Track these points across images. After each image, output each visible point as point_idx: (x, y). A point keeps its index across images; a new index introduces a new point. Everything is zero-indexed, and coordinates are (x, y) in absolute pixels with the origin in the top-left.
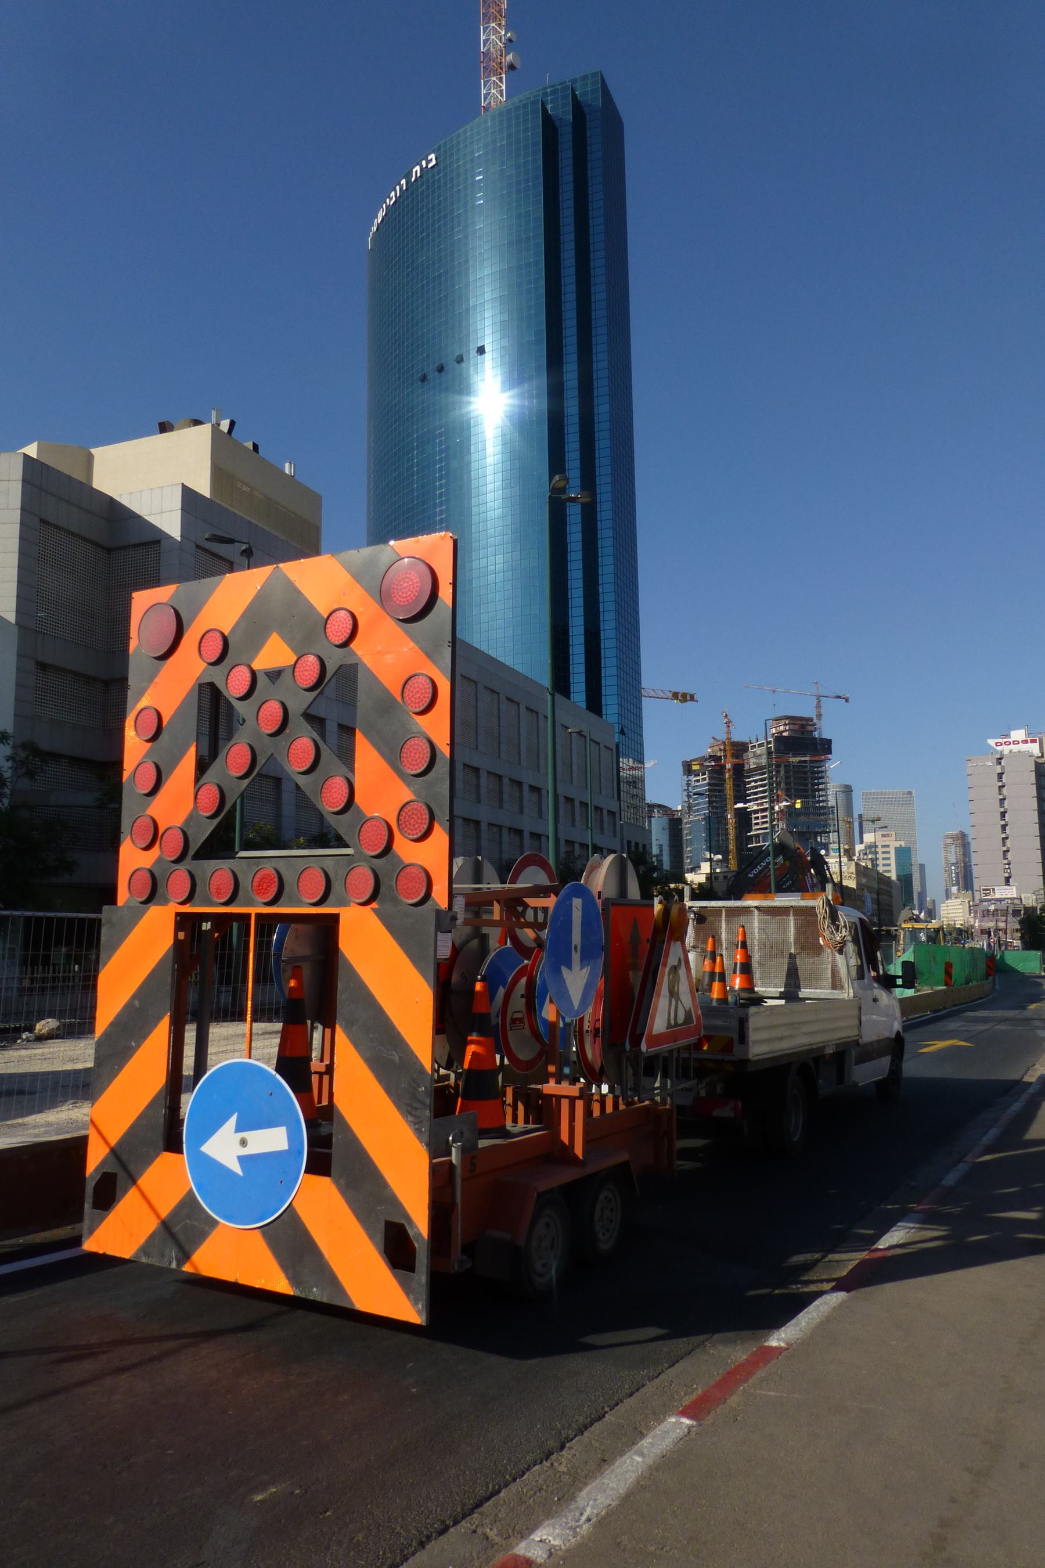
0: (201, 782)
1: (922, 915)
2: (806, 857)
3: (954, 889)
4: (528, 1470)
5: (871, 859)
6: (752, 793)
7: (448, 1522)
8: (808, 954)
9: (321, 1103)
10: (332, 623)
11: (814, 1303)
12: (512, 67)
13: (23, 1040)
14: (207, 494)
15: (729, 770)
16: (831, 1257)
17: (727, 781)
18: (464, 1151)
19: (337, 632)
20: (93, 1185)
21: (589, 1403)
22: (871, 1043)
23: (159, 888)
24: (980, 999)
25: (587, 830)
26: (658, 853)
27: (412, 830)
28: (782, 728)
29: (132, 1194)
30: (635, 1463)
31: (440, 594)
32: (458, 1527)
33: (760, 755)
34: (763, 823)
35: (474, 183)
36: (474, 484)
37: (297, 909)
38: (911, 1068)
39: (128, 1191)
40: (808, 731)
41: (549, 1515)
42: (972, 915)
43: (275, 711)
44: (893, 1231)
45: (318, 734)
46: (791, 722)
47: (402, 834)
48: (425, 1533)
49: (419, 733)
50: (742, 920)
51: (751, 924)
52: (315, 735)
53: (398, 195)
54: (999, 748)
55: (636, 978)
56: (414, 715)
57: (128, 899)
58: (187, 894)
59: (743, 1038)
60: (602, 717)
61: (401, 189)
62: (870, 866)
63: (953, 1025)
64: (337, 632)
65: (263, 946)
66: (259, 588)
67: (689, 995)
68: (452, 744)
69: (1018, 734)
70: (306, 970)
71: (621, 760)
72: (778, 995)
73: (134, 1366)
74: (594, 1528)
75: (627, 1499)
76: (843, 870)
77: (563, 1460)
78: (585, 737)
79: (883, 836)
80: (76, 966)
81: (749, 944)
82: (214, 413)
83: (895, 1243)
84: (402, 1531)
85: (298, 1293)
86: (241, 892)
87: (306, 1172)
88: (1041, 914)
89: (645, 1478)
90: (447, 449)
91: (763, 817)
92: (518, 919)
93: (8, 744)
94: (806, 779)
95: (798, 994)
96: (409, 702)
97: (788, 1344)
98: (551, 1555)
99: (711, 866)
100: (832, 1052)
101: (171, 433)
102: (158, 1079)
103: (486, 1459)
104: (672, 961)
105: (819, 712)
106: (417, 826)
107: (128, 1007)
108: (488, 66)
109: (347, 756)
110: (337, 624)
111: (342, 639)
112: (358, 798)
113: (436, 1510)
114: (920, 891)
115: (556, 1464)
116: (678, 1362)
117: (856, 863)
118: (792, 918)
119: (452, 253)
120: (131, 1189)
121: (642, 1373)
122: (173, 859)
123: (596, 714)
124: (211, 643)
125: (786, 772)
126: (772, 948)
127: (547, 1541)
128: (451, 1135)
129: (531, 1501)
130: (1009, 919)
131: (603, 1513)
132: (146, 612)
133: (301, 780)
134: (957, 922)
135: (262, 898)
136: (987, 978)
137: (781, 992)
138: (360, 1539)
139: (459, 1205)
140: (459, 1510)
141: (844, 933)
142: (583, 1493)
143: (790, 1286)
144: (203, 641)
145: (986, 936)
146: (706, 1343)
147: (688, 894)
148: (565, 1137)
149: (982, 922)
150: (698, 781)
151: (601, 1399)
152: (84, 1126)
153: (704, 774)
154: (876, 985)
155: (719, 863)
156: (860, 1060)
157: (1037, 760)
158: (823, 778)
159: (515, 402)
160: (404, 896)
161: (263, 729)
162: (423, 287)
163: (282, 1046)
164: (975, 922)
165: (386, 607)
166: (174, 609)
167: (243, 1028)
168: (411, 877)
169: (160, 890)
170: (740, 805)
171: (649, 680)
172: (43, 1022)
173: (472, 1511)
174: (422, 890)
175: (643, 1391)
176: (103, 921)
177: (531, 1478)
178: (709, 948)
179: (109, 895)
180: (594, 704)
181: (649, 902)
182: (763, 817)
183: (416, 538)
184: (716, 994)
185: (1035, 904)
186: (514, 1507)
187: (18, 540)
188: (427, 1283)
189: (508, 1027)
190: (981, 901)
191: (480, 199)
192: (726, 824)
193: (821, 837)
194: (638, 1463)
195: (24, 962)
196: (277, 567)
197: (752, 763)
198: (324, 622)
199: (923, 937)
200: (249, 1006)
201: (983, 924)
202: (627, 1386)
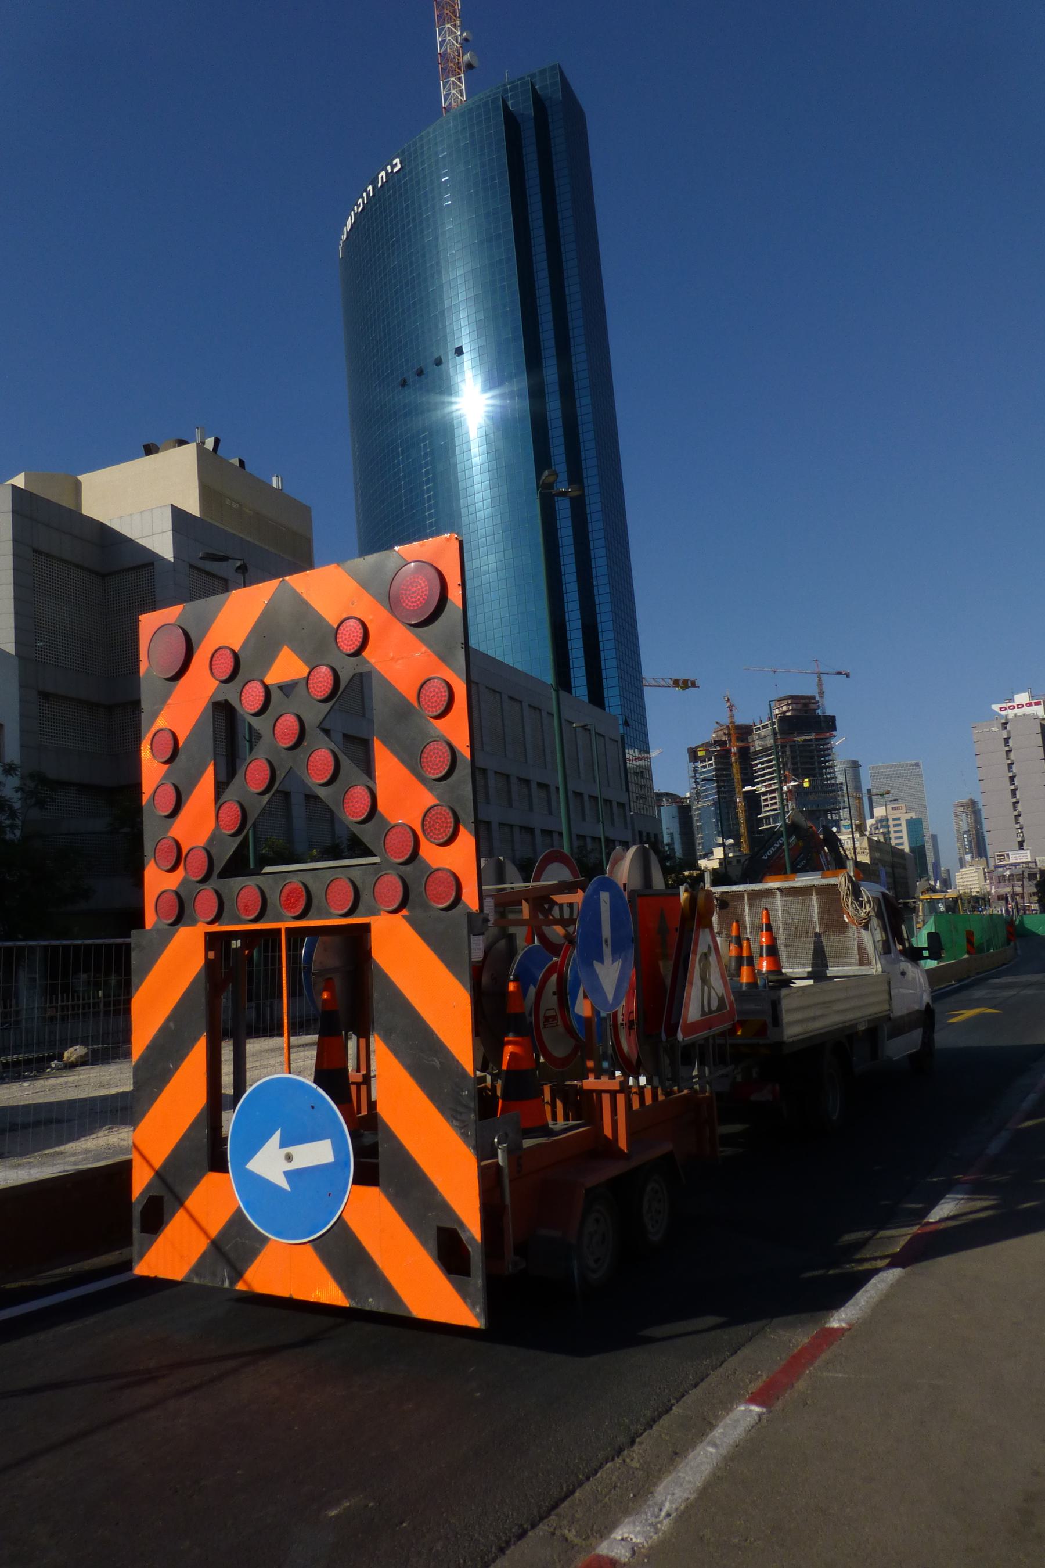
0: (221, 801)
2: (818, 835)
3: (968, 857)
4: (600, 1467)
5: (882, 833)
8: (833, 932)
10: (342, 633)
12: (470, 66)
13: (53, 1069)
14: (198, 516)
15: (735, 754)
16: (882, 1233)
17: (734, 764)
18: (510, 1152)
19: (348, 641)
21: (655, 1397)
22: (902, 1017)
23: (186, 909)
25: (599, 821)
26: (669, 841)
27: (437, 835)
28: (785, 708)
29: (180, 1215)
30: (709, 1454)
31: (450, 596)
32: (537, 1530)
33: (765, 737)
34: (772, 804)
36: (461, 485)
37: (326, 921)
38: (942, 1039)
39: (177, 1213)
40: (811, 709)
41: (626, 1512)
42: (988, 881)
43: (291, 725)
44: (942, 1204)
47: (430, 841)
48: (503, 1539)
49: (438, 736)
50: (765, 902)
53: (365, 202)
54: (1003, 713)
55: (666, 968)
56: (431, 720)
57: (156, 923)
58: (215, 914)
59: (776, 1020)
61: (368, 195)
62: (882, 840)
63: (979, 993)
64: (348, 641)
65: (293, 959)
66: (266, 602)
67: (721, 982)
68: (472, 746)
69: (1022, 698)
70: (338, 982)
71: (627, 751)
72: (806, 975)
75: (704, 1492)
76: (856, 846)
78: (589, 730)
79: (893, 809)
82: (198, 433)
85: (354, 1305)
86: (269, 908)
87: (353, 1183)
91: (772, 798)
92: (546, 916)
93: (17, 775)
94: (812, 757)
96: (426, 706)
98: (634, 1553)
99: (724, 851)
100: (864, 1028)
101: (156, 455)
102: (199, 1099)
104: (702, 949)
105: (821, 690)
106: (442, 831)
107: (164, 1029)
109: (368, 767)
110: (348, 634)
111: (324, 694)
112: (380, 807)
113: (512, 1515)
115: (628, 1460)
116: (739, 1349)
117: (868, 838)
118: (814, 897)
119: (424, 256)
124: (222, 661)
125: (792, 752)
127: (629, 1539)
128: (496, 1137)
130: (1025, 883)
131: (682, 1507)
132: (158, 629)
133: (322, 792)
134: (972, 890)
136: (1008, 944)
137: (808, 972)
141: (868, 909)
142: (660, 1488)
144: (214, 659)
146: (766, 1329)
147: (709, 880)
148: (608, 1131)
150: (705, 767)
151: (667, 1391)
153: (710, 759)
154: (902, 958)
155: (732, 848)
156: (891, 1036)
158: (830, 755)
160: (434, 902)
161: (280, 744)
162: (396, 292)
164: (991, 889)
166: (182, 628)
167: (281, 1042)
169: (187, 912)
170: (748, 788)
172: (71, 1050)
173: (548, 1514)
174: (452, 895)
175: (708, 1379)
176: (132, 946)
177: (604, 1476)
178: (734, 933)
179: (137, 919)
181: (674, 891)
182: (772, 798)
183: (421, 542)
184: (745, 978)
189: (542, 1026)
190: (997, 867)
191: (447, 200)
192: (736, 807)
196: (284, 580)
197: (757, 745)
198: (334, 632)
199: (942, 907)
201: (999, 890)
202: (691, 1377)
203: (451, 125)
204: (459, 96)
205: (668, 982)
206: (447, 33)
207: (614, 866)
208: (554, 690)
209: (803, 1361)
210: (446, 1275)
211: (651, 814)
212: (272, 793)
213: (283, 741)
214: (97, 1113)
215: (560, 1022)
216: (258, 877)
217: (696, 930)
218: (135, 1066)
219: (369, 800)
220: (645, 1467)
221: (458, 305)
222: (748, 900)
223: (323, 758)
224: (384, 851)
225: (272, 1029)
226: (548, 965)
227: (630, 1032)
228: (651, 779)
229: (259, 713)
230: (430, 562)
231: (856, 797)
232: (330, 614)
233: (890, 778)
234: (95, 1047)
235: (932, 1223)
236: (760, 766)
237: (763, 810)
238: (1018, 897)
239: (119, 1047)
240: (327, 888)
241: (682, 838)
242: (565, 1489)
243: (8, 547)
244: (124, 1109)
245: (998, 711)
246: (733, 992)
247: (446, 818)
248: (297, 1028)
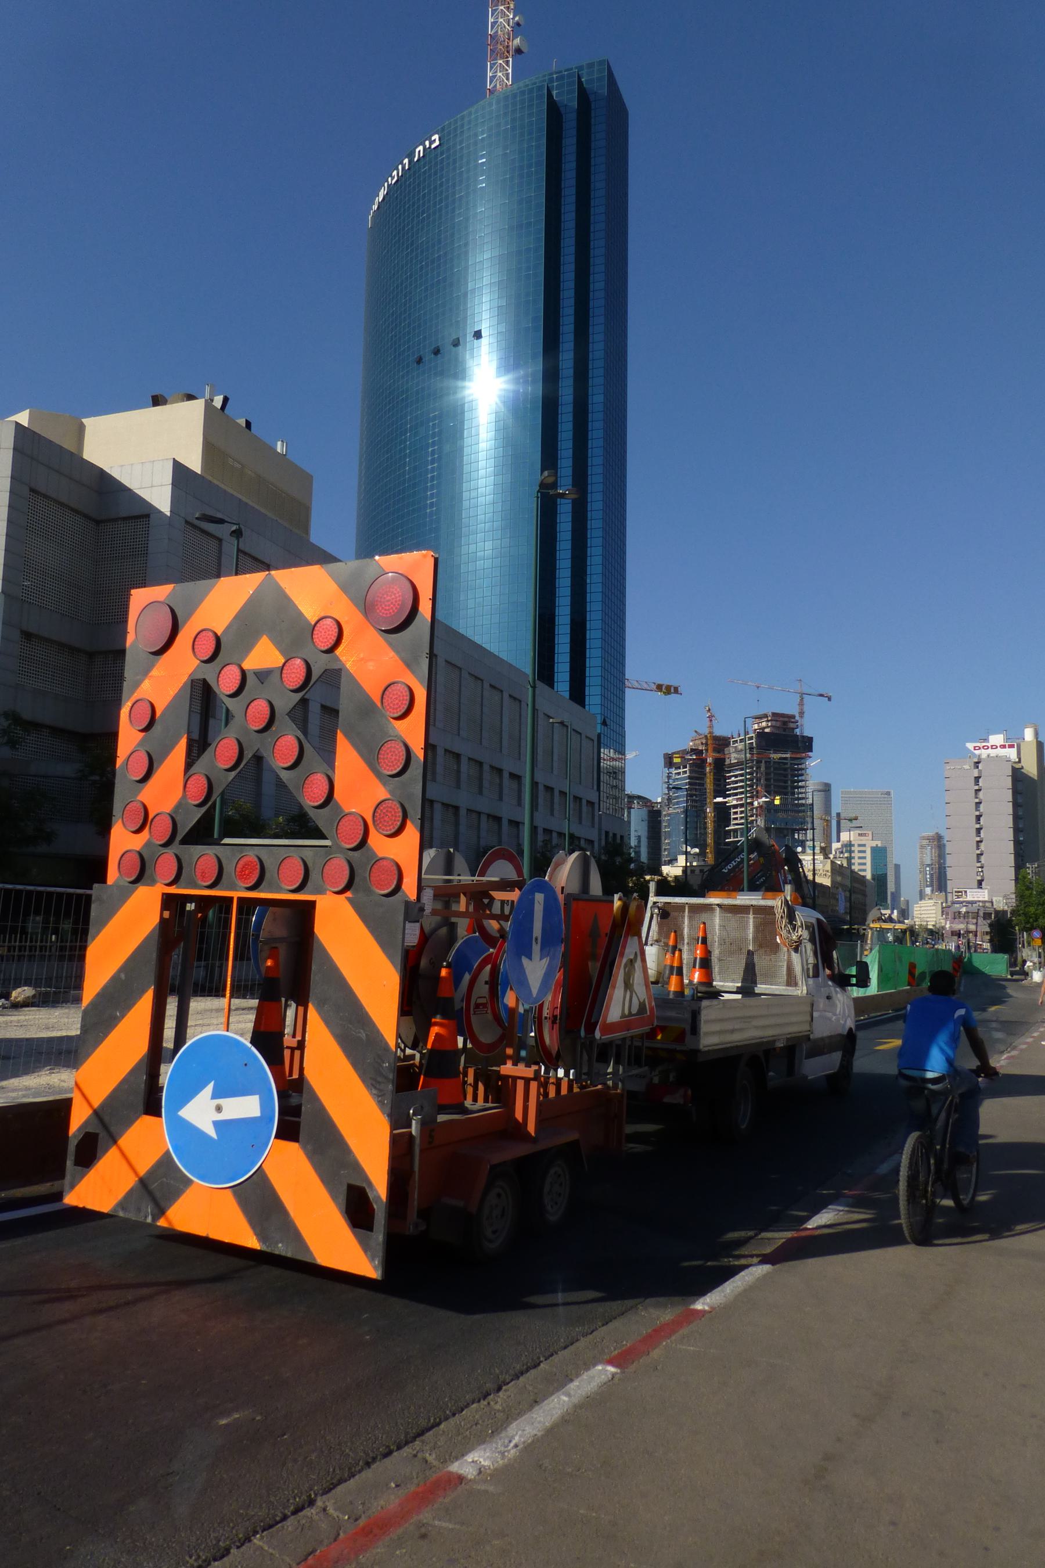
0: (192, 770)
1: (895, 915)
3: (928, 890)
5: (847, 858)
6: (732, 788)
7: (392, 1447)
12: (519, 51)
14: (199, 473)
15: (710, 764)
17: (708, 775)
18: (423, 1124)
19: (323, 639)
21: (526, 1353)
22: (822, 1039)
23: (147, 868)
26: (636, 844)
28: (764, 724)
29: (113, 1152)
30: (562, 1401)
31: (421, 609)
32: (401, 1451)
35: (477, 165)
36: (466, 469)
38: (862, 1064)
46: (773, 718)
47: (378, 831)
49: (396, 736)
50: (704, 917)
51: (712, 920)
52: (299, 734)
53: (400, 174)
54: (977, 752)
58: (173, 877)
59: (695, 1029)
60: (584, 707)
61: (403, 168)
62: (845, 865)
64: (323, 639)
66: (251, 592)
69: (997, 739)
70: (283, 951)
71: (602, 750)
72: (735, 990)
73: (110, 1309)
74: (520, 1453)
75: (551, 1432)
79: (860, 835)
80: (54, 937)
81: (709, 937)
82: (207, 389)
83: (823, 1224)
84: (351, 1453)
85: (264, 1248)
86: (224, 876)
87: (276, 1137)
88: (1011, 917)
89: (569, 1414)
90: (440, 433)
94: (786, 776)
95: (754, 989)
96: (388, 707)
97: (711, 1308)
98: (480, 1472)
100: (782, 1045)
101: (164, 406)
102: (141, 1047)
103: (429, 1396)
105: (802, 710)
106: (390, 823)
107: (115, 979)
109: (328, 755)
110: (323, 632)
112: (336, 796)
113: (382, 1437)
115: (492, 1403)
116: (611, 1321)
117: (831, 861)
118: (751, 916)
119: (453, 235)
120: (111, 1148)
124: (205, 642)
125: (766, 768)
129: (468, 1432)
130: (979, 921)
131: (529, 1441)
133: (285, 775)
135: (244, 883)
137: (738, 987)
139: (417, 1174)
141: (800, 933)
142: (514, 1425)
143: (722, 1259)
145: (956, 937)
150: (679, 774)
151: (538, 1350)
152: (71, 1090)
153: (685, 767)
154: (830, 983)
155: (696, 857)
156: (811, 1054)
157: (1014, 765)
159: (510, 387)
160: (377, 887)
162: (421, 268)
164: (946, 924)
165: (371, 621)
167: (223, 1002)
168: (383, 870)
169: (148, 872)
170: (719, 800)
172: (19, 990)
173: (414, 1439)
175: (577, 1344)
176: (93, 898)
178: (671, 943)
179: (97, 870)
180: (578, 694)
181: (609, 898)
183: (400, 555)
184: (673, 987)
185: (1006, 908)
187: (7, 509)
188: (383, 1242)
189: (472, 1012)
190: (953, 903)
191: (482, 182)
192: (705, 818)
193: (799, 833)
194: (564, 1401)
196: (270, 574)
197: (733, 758)
199: (890, 937)
200: (229, 983)
201: (953, 925)
202: (562, 1340)
204: (505, 79)
206: (500, 14)
211: (620, 816)
219: (327, 787)
221: (481, 288)
224: (335, 835)
225: (217, 991)
228: (623, 781)
230: (406, 574)
232: (310, 612)
235: (810, 1229)
236: (733, 779)
237: (732, 823)
238: (971, 934)
242: (432, 1421)
243: (6, 484)
244: (69, 1052)
245: (972, 749)
246: (655, 999)
247: (395, 812)
248: (240, 990)
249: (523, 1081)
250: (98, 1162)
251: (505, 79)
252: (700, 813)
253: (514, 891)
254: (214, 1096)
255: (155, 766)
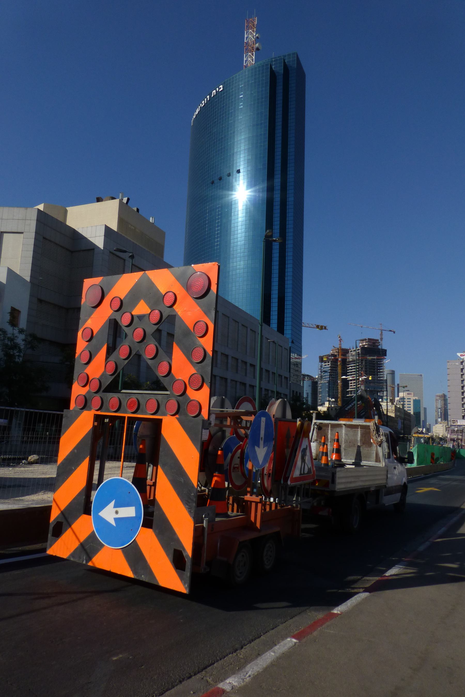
0: (109, 360)
3: (439, 420)
5: (402, 404)
6: (349, 372)
7: (192, 674)
8: (366, 446)
9: (150, 498)
10: (166, 298)
11: (355, 597)
12: (258, 49)
13: (23, 464)
15: (340, 361)
17: (339, 366)
18: (209, 522)
20: (53, 526)
22: (392, 487)
23: (88, 403)
24: (447, 470)
28: (364, 343)
29: (69, 531)
31: (212, 288)
32: (196, 676)
33: (354, 355)
35: (239, 99)
36: (232, 229)
38: (410, 499)
41: (234, 673)
45: (158, 343)
46: (369, 341)
47: (191, 388)
49: (200, 345)
50: (338, 430)
51: (342, 431)
52: (156, 343)
53: (205, 102)
54: (462, 357)
55: (288, 452)
57: (75, 407)
59: (333, 481)
61: (207, 100)
62: (401, 407)
63: (432, 481)
66: (137, 281)
70: (147, 442)
71: (291, 354)
72: (352, 463)
74: (251, 679)
75: (266, 670)
76: (388, 408)
77: (242, 653)
79: (408, 394)
82: (120, 195)
83: (393, 574)
85: (136, 577)
86: (122, 407)
87: (142, 526)
89: (274, 661)
90: (221, 214)
91: (354, 383)
93: (24, 334)
96: (196, 332)
98: (233, 688)
99: (329, 404)
100: (373, 489)
102: (83, 484)
104: (303, 446)
107: (72, 452)
108: (248, 48)
109: (169, 353)
110: (168, 298)
111: (170, 304)
112: (173, 371)
113: (187, 669)
114: (424, 419)
115: (239, 654)
116: (294, 617)
118: (359, 430)
121: (278, 620)
122: (94, 391)
123: (281, 334)
124: (116, 302)
125: (365, 363)
126: (350, 442)
129: (227, 668)
131: (256, 674)
133: (150, 362)
137: (353, 462)
138: (155, 678)
140: (197, 670)
141: (382, 438)
142: (249, 666)
144: (112, 301)
145: (453, 441)
148: (253, 519)
149: (451, 435)
150: (326, 365)
152: (51, 502)
153: (329, 362)
154: (395, 461)
155: (333, 403)
159: (252, 194)
160: (190, 413)
163: (135, 473)
164: (448, 435)
166: (100, 286)
169: (88, 404)
170: (344, 377)
171: (307, 318)
172: (32, 456)
173: (202, 671)
174: (197, 411)
175: (278, 627)
176: (64, 416)
178: (323, 441)
180: (281, 329)
184: (323, 462)
186: (219, 670)
189: (232, 471)
190: (451, 426)
191: (241, 105)
192: (338, 385)
193: (380, 393)
194: (272, 655)
195: (24, 430)
196: (145, 272)
197: (350, 359)
199: (422, 441)
200: (123, 455)
201: (451, 436)
202: (271, 625)
203: (247, 73)
204: (251, 61)
205: (288, 458)
207: (270, 407)
208: (260, 325)
209: (318, 624)
210: (175, 570)
212: (129, 359)
213: (136, 338)
214: (39, 485)
215: (240, 470)
216: (119, 394)
217: (302, 438)
218: (58, 466)
220: (245, 658)
221: (240, 151)
222: (331, 427)
223: (152, 348)
225: (117, 459)
226: (237, 446)
227: (269, 478)
228: (301, 368)
229: (127, 326)
231: (392, 387)
233: (413, 380)
234: (42, 456)
236: (350, 368)
237: (350, 388)
238: (459, 440)
239: (52, 458)
240: (147, 402)
241: (312, 396)
242: (210, 662)
244: (52, 485)
249: (255, 503)
250: (62, 535)
251: (251, 61)
252: (336, 383)
253: (252, 416)
254: (115, 507)
255: (93, 357)
